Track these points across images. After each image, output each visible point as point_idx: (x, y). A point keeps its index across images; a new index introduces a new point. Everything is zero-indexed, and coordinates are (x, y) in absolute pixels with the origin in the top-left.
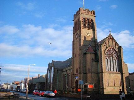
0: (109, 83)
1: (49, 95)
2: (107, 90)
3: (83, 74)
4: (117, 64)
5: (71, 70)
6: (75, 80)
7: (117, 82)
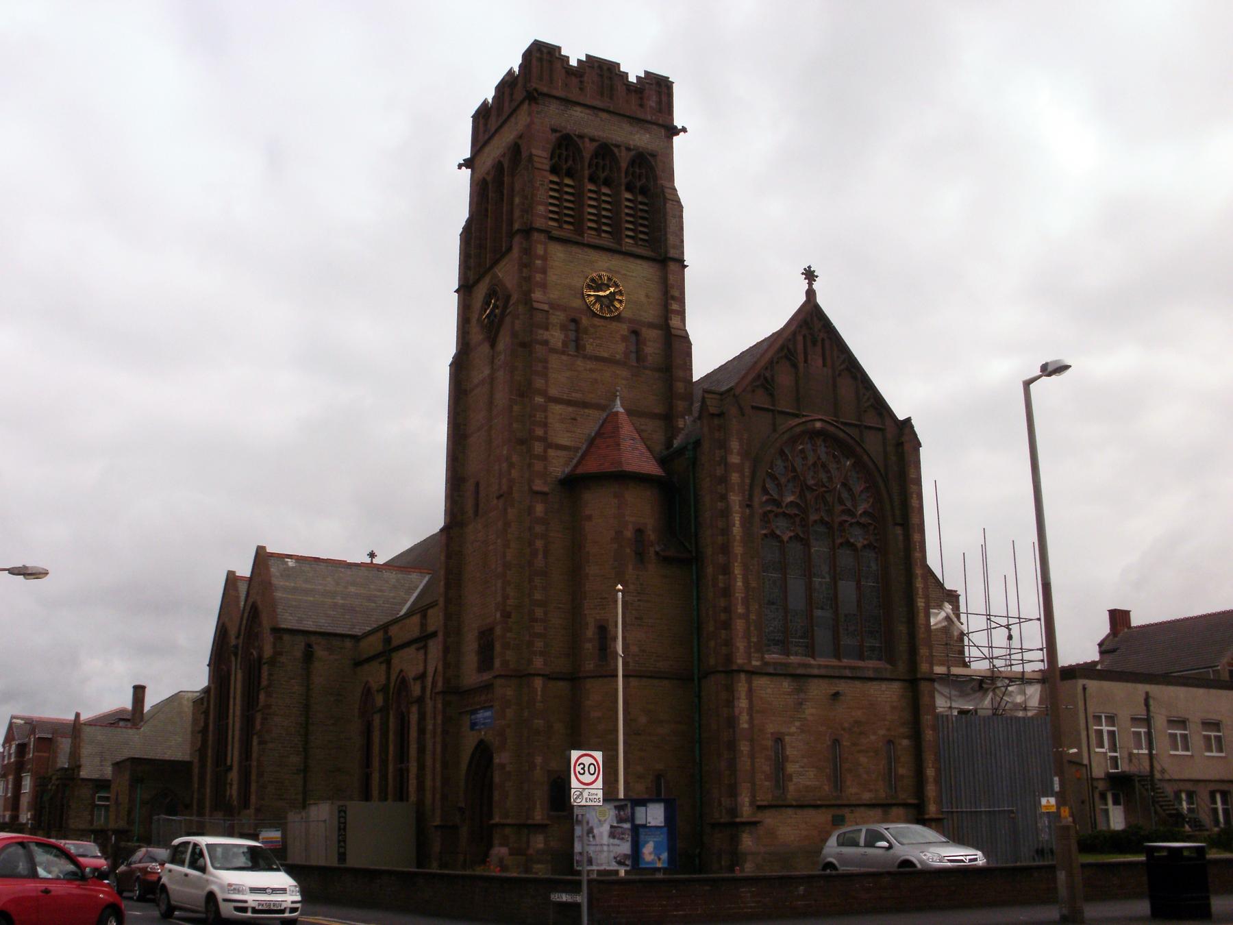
0: (858, 684)
3: (538, 683)
5: (435, 647)
6: (469, 742)
7: (863, 759)
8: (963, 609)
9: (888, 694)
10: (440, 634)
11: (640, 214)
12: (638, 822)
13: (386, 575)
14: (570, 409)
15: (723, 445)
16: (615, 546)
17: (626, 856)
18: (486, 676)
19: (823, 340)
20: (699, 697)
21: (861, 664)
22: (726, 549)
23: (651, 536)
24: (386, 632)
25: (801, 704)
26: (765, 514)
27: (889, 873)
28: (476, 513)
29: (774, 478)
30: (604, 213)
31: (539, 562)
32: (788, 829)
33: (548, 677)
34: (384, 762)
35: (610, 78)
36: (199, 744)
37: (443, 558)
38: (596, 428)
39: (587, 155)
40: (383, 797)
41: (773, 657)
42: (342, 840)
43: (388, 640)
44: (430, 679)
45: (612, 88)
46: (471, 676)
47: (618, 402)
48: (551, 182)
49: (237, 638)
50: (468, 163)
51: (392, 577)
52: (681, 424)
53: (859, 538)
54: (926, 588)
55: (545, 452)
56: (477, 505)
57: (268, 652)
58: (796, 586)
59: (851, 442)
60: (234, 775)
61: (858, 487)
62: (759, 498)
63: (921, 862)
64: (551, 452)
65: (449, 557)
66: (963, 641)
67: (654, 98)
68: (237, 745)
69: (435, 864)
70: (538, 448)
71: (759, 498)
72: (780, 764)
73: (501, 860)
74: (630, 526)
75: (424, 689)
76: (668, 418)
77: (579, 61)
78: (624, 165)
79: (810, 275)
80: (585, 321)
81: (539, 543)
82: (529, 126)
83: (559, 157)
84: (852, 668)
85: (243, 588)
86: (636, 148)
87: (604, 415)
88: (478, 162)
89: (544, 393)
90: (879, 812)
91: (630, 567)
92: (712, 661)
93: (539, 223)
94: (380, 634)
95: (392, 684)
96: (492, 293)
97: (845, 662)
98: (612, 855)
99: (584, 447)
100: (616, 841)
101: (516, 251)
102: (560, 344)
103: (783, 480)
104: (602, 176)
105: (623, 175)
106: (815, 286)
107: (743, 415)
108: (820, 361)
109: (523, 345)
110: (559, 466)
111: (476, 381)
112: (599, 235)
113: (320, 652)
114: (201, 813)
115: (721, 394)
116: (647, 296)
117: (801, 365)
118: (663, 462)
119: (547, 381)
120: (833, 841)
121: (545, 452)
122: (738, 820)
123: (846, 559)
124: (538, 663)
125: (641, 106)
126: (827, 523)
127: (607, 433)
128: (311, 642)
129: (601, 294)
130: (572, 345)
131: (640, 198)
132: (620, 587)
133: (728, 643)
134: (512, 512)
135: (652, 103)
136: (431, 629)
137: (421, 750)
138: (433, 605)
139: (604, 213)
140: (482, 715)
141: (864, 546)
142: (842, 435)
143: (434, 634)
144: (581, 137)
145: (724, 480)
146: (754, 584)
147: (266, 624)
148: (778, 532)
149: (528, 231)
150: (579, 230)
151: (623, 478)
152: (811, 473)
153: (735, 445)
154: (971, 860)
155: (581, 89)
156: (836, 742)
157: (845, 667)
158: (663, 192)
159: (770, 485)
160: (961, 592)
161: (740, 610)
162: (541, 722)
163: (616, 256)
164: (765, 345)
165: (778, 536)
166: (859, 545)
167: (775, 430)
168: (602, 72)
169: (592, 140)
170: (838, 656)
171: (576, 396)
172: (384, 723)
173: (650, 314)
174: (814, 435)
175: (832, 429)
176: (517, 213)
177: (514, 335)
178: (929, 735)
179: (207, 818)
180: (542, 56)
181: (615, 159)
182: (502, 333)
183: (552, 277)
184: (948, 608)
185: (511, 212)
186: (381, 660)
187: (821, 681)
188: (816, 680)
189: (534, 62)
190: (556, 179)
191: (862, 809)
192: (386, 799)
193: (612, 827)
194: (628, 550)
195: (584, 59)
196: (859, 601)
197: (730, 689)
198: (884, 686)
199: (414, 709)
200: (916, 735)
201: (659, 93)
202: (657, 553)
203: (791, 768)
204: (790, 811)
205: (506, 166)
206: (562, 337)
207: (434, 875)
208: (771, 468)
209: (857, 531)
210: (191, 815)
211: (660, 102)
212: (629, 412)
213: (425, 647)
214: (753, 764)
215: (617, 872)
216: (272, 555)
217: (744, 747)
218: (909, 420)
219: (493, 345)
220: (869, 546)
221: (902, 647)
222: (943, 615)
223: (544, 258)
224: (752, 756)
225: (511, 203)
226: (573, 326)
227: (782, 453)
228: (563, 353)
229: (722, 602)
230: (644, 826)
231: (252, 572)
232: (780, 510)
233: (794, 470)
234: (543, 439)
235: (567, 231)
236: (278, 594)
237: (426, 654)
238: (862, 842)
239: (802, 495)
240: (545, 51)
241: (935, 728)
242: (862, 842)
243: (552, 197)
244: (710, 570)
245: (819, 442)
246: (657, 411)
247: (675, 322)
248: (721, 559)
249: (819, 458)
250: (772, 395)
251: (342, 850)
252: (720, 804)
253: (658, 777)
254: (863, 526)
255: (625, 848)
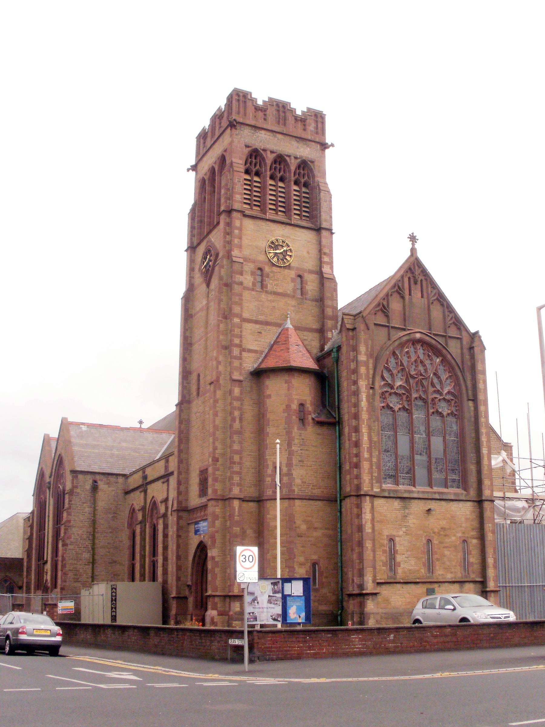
0: (443, 503)
1: (17, 640)
2: (387, 601)
3: (236, 503)
4: (149, 667)
7: (447, 552)
8: (515, 454)
9: (464, 511)
10: (176, 473)
11: (304, 200)
12: (286, 593)
13: (146, 435)
14: (257, 326)
15: (355, 349)
16: (286, 414)
17: (278, 615)
18: (204, 500)
19: (421, 281)
20: (341, 512)
21: (445, 490)
22: (356, 416)
23: (309, 407)
24: (144, 472)
25: (406, 516)
26: (383, 393)
27: (450, 626)
28: (198, 394)
29: (388, 370)
30: (280, 199)
31: (237, 425)
32: (396, 598)
33: (242, 500)
34: (143, 557)
35: (284, 112)
36: (27, 547)
37: (177, 423)
38: (274, 339)
39: (269, 162)
40: (143, 578)
41: (388, 486)
42: (114, 608)
43: (145, 477)
44: (170, 503)
45: (285, 119)
46: (194, 500)
47: (289, 321)
48: (245, 179)
49: (50, 477)
50: (194, 168)
51: (150, 436)
52: (329, 335)
53: (444, 408)
54: (489, 441)
55: (241, 354)
56: (198, 389)
57: (68, 486)
58: (403, 441)
59: (439, 346)
60: (48, 567)
61: (444, 376)
62: (379, 382)
63: (473, 619)
64: (244, 354)
65: (181, 422)
66: (514, 475)
67: (313, 125)
68: (50, 546)
69: (172, 622)
70: (236, 351)
71: (379, 382)
72: (392, 554)
73: (212, 619)
74: (296, 402)
75: (167, 508)
76: (321, 331)
77: (303, 112)
78: (293, 168)
79: (413, 239)
80: (267, 269)
81: (237, 413)
82: (231, 143)
83: (251, 164)
84: (439, 493)
85: (54, 445)
86: (301, 157)
87: (280, 330)
88: (199, 167)
89: (240, 316)
90: (457, 586)
91: (296, 428)
92: (348, 489)
93: (237, 206)
94: (140, 473)
95: (148, 506)
96: (208, 252)
97: (435, 489)
98: (270, 614)
99: (266, 351)
100: (272, 605)
101: (222, 225)
102: (251, 284)
103: (395, 372)
104: (279, 175)
105: (292, 174)
106: (417, 246)
107: (368, 329)
108: (420, 295)
109: (226, 285)
110: (250, 363)
111: (198, 309)
112: (277, 214)
113: (102, 485)
114: (28, 591)
115: (355, 316)
116: (308, 252)
117: (407, 297)
118: (319, 360)
119: (242, 308)
120: (419, 605)
121: (241, 354)
122: (364, 592)
123: (436, 422)
124: (236, 491)
125: (305, 130)
126: (423, 399)
127: (281, 341)
128: (96, 479)
129: (278, 251)
130: (259, 285)
131: (304, 190)
132: (278, 441)
133: (358, 477)
134: (219, 393)
135: (311, 127)
136: (171, 470)
137: (165, 548)
138: (172, 454)
139: (280, 199)
140: (203, 525)
141: (448, 414)
142: (433, 342)
143: (172, 473)
144: (264, 150)
145: (355, 371)
146: (375, 439)
147: (67, 468)
148: (391, 405)
149: (229, 212)
150: (264, 211)
151: (290, 370)
152: (414, 367)
153: (362, 349)
154: (505, 618)
155: (265, 119)
156: (429, 541)
157: (435, 493)
158: (318, 185)
159: (386, 375)
160: (514, 444)
161: (366, 455)
162: (238, 529)
163: (288, 227)
164: (385, 283)
165: (391, 408)
166: (445, 414)
167: (389, 339)
168: (281, 109)
169: (272, 152)
170: (430, 485)
171: (261, 318)
172: (143, 532)
173: (310, 264)
174: (415, 342)
175: (427, 338)
176: (223, 200)
177: (221, 278)
178: (489, 537)
179: (32, 595)
180: (239, 99)
181: (287, 165)
182: (214, 276)
183: (245, 241)
184: (504, 454)
185: (219, 200)
186: (141, 490)
187: (419, 501)
188: (416, 501)
189: (234, 102)
190: (248, 177)
191: (446, 584)
192: (144, 580)
193: (269, 596)
194: (294, 417)
195: (306, 110)
196: (445, 451)
197: (359, 506)
198: (461, 504)
199: (161, 521)
200: (482, 537)
201: (317, 122)
202: (313, 419)
203: (399, 558)
204: (398, 586)
205: (216, 170)
206: (252, 279)
207: (172, 630)
208: (387, 363)
209: (443, 404)
210: (23, 593)
211: (317, 128)
212: (297, 328)
213: (168, 481)
214: (374, 557)
215: (276, 626)
216: (72, 423)
217: (368, 544)
218: (477, 333)
219: (208, 285)
220: (452, 414)
221: (472, 479)
222: (500, 459)
223: (240, 229)
224: (374, 551)
225: (219, 193)
226: (259, 272)
227: (394, 354)
228: (253, 290)
229: (355, 451)
230: (290, 596)
231: (59, 435)
232: (393, 391)
233: (402, 365)
234: (239, 346)
235: (256, 211)
236: (76, 449)
237: (168, 485)
238: (437, 607)
239: (407, 381)
240: (241, 95)
241: (493, 532)
242: (437, 607)
243: (245, 189)
244: (346, 430)
245: (419, 346)
246: (314, 327)
247: (326, 269)
248: (354, 423)
249: (419, 357)
250: (387, 316)
251: (114, 614)
252: (353, 580)
253: (314, 565)
254: (448, 401)
255: (278, 610)
